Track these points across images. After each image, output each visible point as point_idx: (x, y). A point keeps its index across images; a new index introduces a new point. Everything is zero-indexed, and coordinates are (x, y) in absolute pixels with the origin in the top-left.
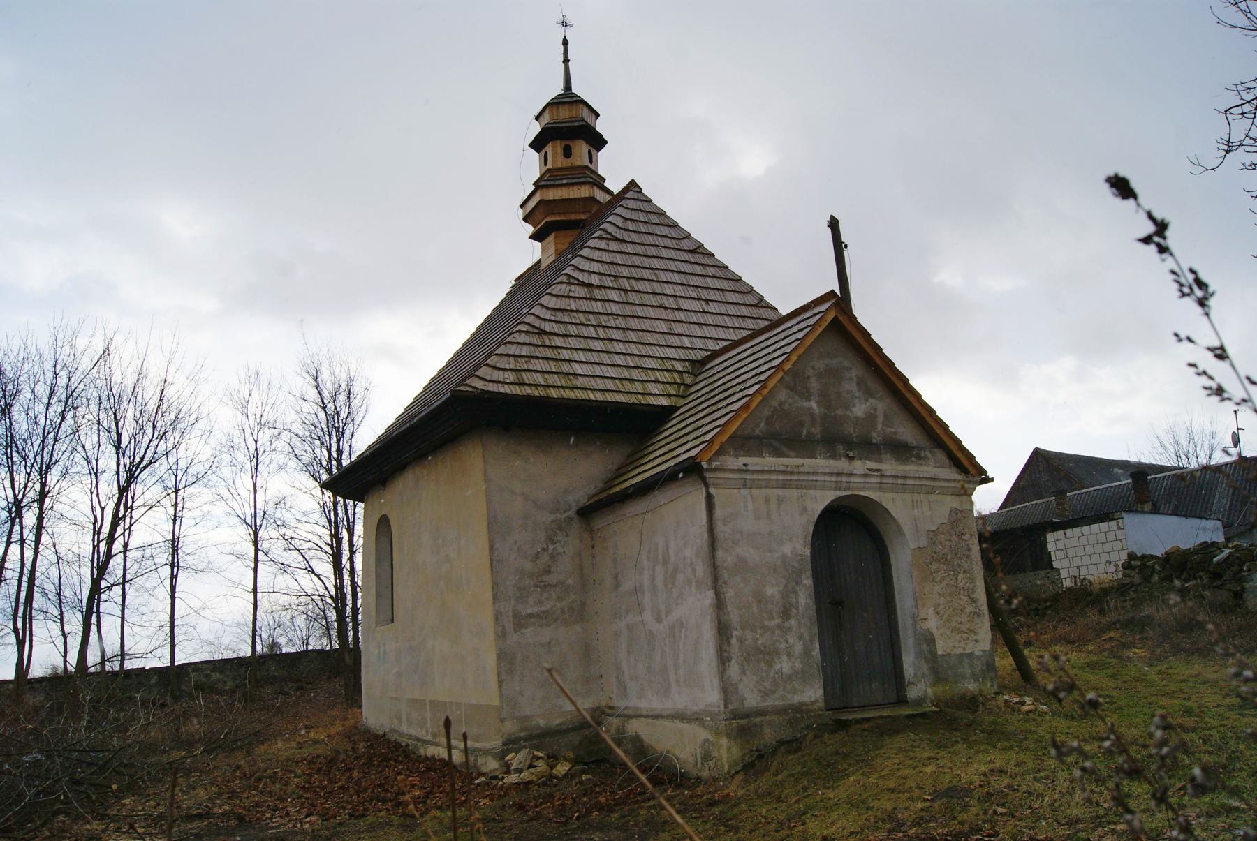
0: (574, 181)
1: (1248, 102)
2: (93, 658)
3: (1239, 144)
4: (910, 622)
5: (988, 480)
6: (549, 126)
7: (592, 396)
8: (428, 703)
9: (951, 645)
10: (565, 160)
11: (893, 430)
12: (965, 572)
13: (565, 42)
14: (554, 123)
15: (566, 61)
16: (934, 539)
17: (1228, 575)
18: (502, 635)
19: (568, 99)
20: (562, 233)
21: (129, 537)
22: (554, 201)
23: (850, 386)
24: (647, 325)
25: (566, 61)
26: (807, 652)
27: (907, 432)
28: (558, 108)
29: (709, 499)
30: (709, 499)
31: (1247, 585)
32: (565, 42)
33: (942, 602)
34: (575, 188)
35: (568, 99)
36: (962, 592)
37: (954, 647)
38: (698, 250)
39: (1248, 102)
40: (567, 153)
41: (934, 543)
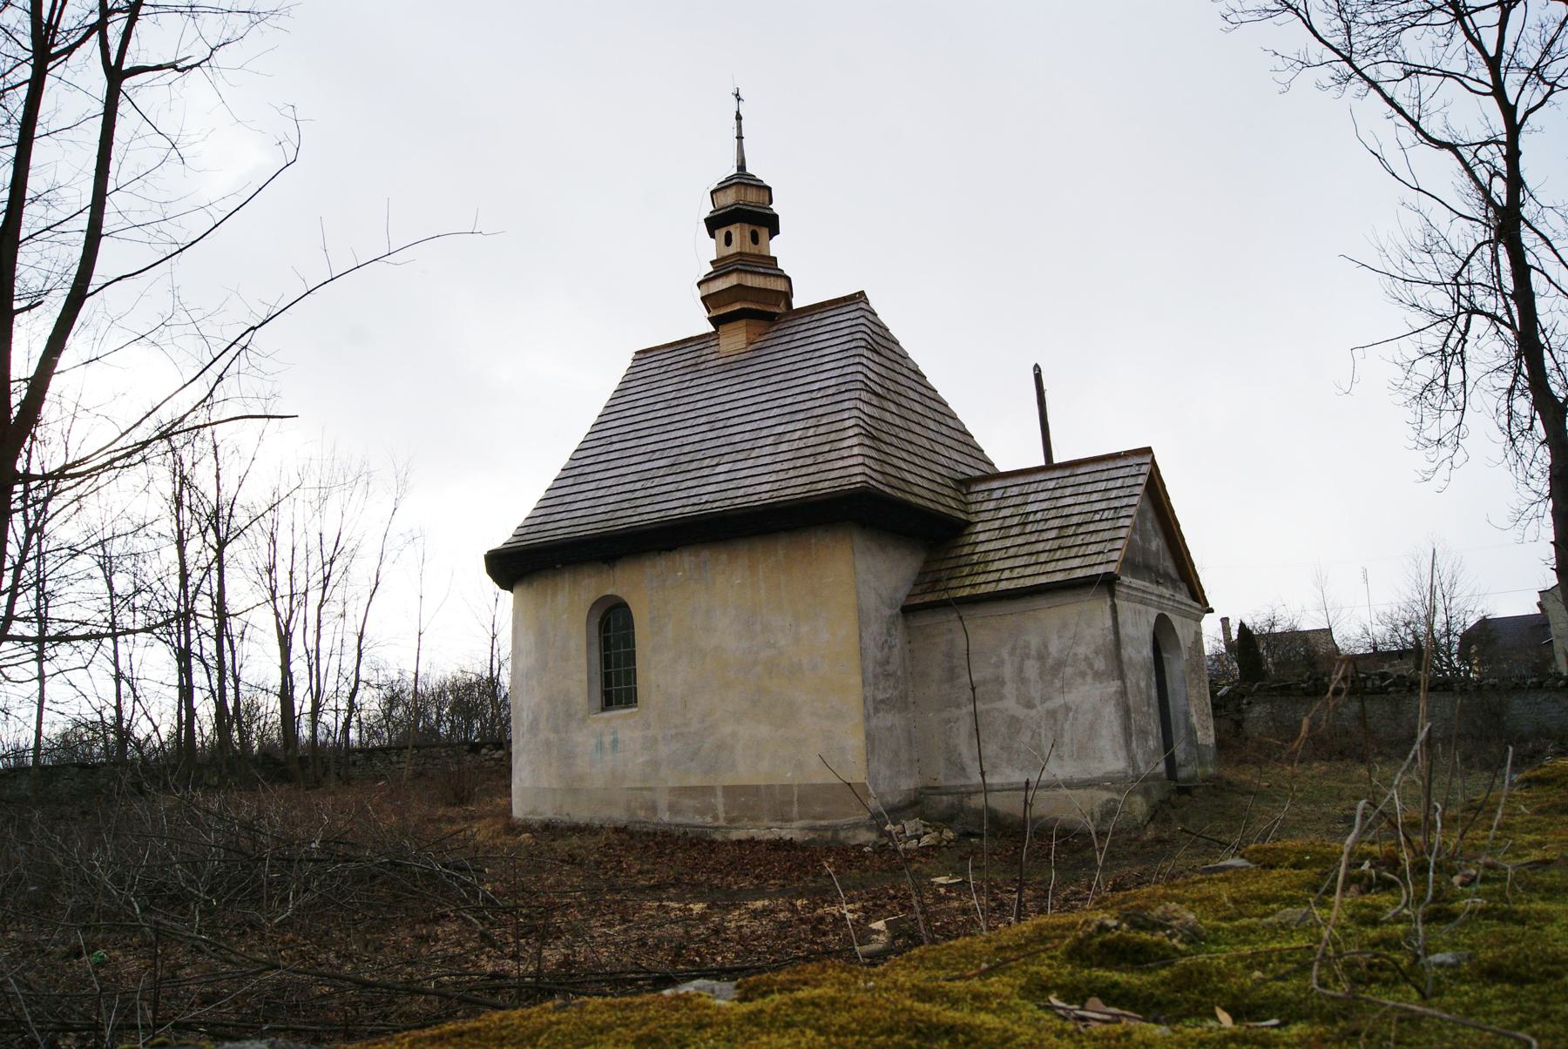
0: (749, 268)
1: (25, 61)
2: (321, 738)
4: (1181, 717)
5: (1211, 611)
7: (941, 509)
8: (719, 793)
10: (752, 245)
13: (739, 117)
15: (740, 138)
17: (1231, 706)
18: (867, 718)
19: (742, 179)
20: (753, 322)
22: (752, 288)
25: (740, 138)
26: (1158, 733)
27: (1168, 565)
29: (1114, 608)
30: (1114, 608)
31: (1246, 716)
32: (739, 117)
34: (772, 279)
35: (742, 179)
38: (918, 373)
39: (25, 61)
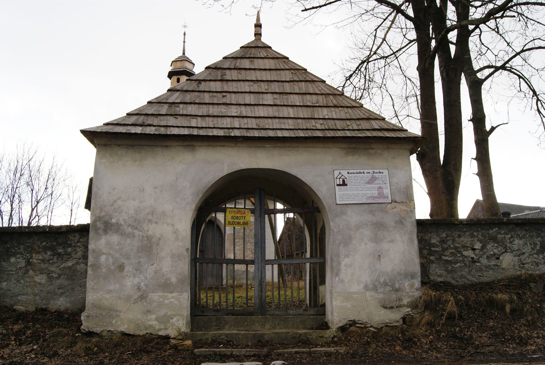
3: (541, 69)
6: (173, 70)
9: (240, 267)
11: (424, 120)
12: (251, 243)
13: (185, 34)
14: (174, 69)
15: (184, 42)
16: (239, 231)
19: (183, 59)
21: (530, 83)
23: (476, 98)
24: (298, 124)
28: (176, 63)
32: (185, 34)
33: (238, 253)
35: (183, 59)
36: (248, 250)
37: (241, 268)
40: (178, 80)
41: (239, 232)
